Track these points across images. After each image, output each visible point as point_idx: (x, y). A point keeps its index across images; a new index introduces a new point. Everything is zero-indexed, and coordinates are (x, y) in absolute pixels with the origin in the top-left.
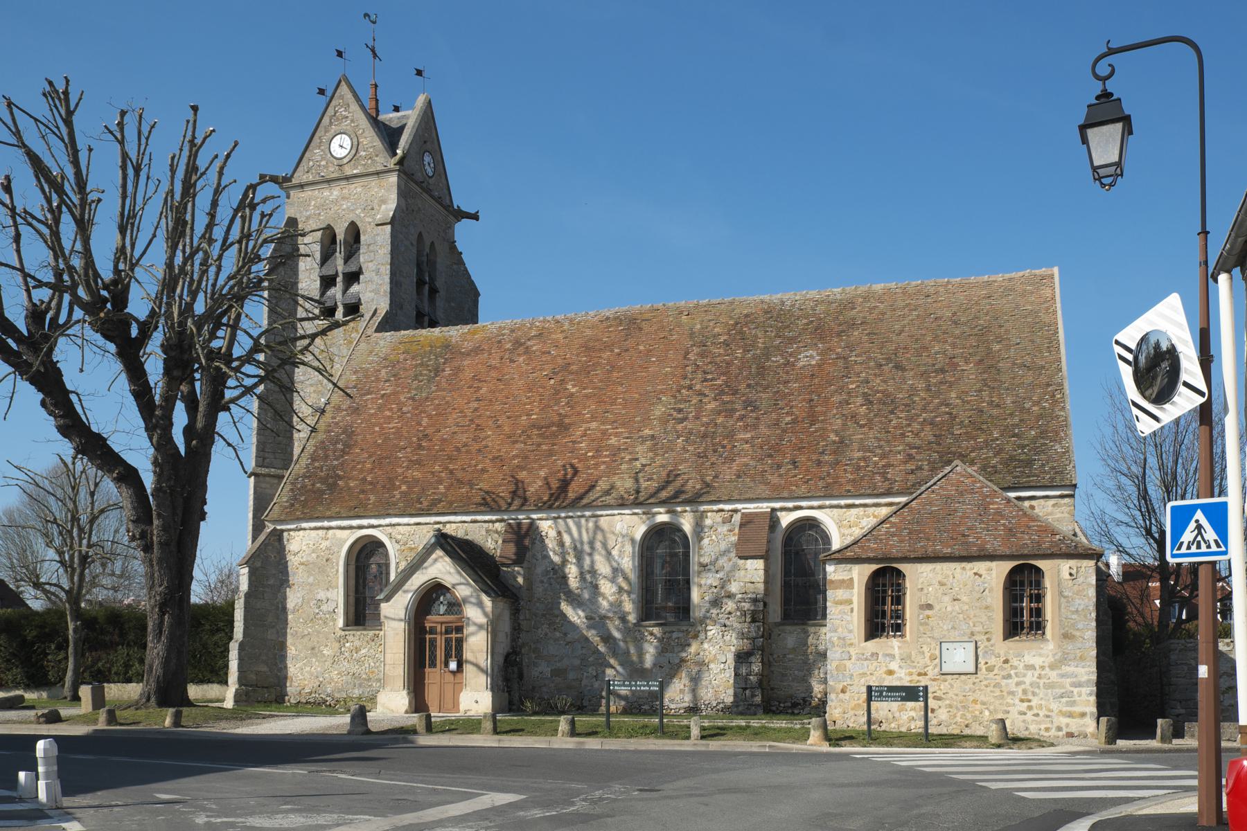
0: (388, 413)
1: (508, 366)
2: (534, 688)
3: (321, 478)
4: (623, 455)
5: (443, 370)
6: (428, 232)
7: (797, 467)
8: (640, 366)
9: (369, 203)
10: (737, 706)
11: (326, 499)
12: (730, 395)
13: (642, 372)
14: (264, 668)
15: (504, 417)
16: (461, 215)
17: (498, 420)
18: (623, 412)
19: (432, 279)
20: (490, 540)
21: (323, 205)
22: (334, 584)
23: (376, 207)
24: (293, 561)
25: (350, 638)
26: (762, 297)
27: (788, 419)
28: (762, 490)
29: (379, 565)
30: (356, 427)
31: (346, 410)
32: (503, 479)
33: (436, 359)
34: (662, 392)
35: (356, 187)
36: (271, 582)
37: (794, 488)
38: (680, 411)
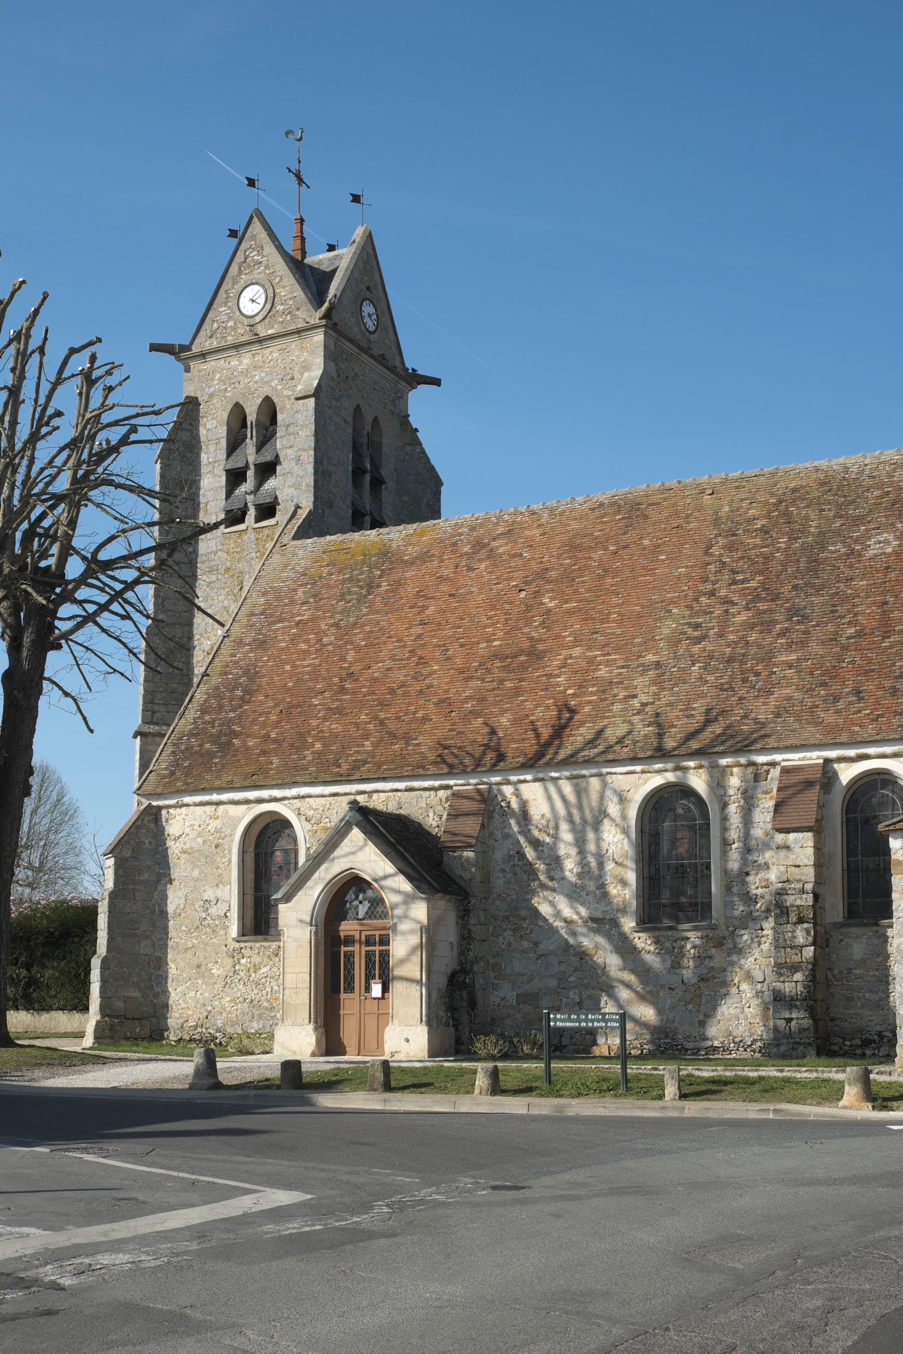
0: (303, 646)
1: (464, 577)
2: (493, 1020)
3: (212, 736)
4: (616, 691)
5: (379, 586)
6: (370, 405)
7: (863, 698)
8: (643, 568)
9: (289, 371)
10: (778, 1046)
11: (216, 763)
12: (768, 601)
13: (645, 576)
14: (135, 993)
15: (456, 645)
16: (416, 379)
17: (448, 650)
18: (619, 631)
19: (376, 467)
20: (431, 815)
21: (230, 379)
22: (226, 879)
23: (297, 376)
24: (174, 848)
25: (247, 952)
26: (816, 463)
27: (851, 631)
28: (811, 733)
29: (286, 852)
30: (262, 667)
31: (249, 644)
32: (451, 730)
33: (370, 571)
34: (672, 602)
35: (271, 353)
36: (145, 876)
37: (857, 728)
38: (697, 626)
